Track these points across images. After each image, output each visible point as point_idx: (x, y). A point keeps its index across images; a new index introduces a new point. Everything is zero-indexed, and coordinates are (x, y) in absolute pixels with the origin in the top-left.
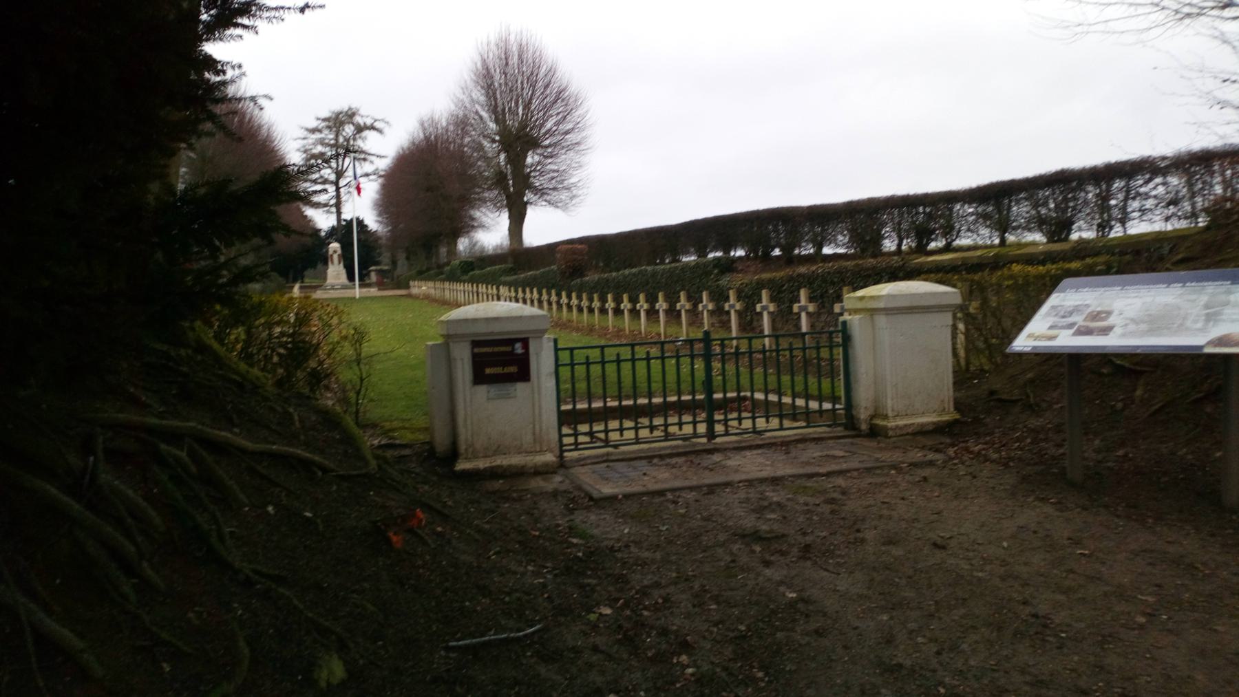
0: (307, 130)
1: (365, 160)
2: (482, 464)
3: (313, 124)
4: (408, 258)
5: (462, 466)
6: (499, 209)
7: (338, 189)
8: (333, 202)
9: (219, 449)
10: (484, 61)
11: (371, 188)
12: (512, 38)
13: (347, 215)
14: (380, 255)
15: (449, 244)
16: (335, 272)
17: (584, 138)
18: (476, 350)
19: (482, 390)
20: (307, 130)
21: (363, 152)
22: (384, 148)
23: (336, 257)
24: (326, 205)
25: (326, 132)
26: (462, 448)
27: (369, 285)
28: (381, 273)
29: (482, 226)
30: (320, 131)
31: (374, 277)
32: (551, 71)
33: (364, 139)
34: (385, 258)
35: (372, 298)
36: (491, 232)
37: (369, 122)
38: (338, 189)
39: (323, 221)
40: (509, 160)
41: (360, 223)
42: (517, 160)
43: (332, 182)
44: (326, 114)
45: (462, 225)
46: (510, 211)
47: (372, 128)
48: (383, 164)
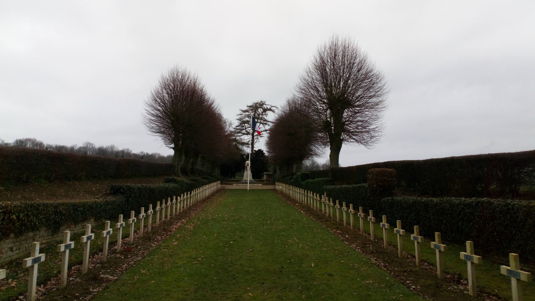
0: (242, 111)
1: (266, 124)
3: (245, 108)
4: (280, 169)
6: (325, 144)
10: (321, 58)
11: (265, 136)
12: (340, 43)
13: (256, 149)
14: (269, 166)
16: (248, 175)
17: (380, 102)
20: (242, 111)
21: (265, 120)
28: (269, 176)
29: (316, 155)
31: (265, 177)
32: (362, 63)
33: (266, 115)
34: (271, 169)
37: (269, 107)
39: (248, 150)
40: (333, 115)
42: (337, 114)
44: (251, 104)
45: (308, 153)
46: (331, 145)
47: (270, 110)
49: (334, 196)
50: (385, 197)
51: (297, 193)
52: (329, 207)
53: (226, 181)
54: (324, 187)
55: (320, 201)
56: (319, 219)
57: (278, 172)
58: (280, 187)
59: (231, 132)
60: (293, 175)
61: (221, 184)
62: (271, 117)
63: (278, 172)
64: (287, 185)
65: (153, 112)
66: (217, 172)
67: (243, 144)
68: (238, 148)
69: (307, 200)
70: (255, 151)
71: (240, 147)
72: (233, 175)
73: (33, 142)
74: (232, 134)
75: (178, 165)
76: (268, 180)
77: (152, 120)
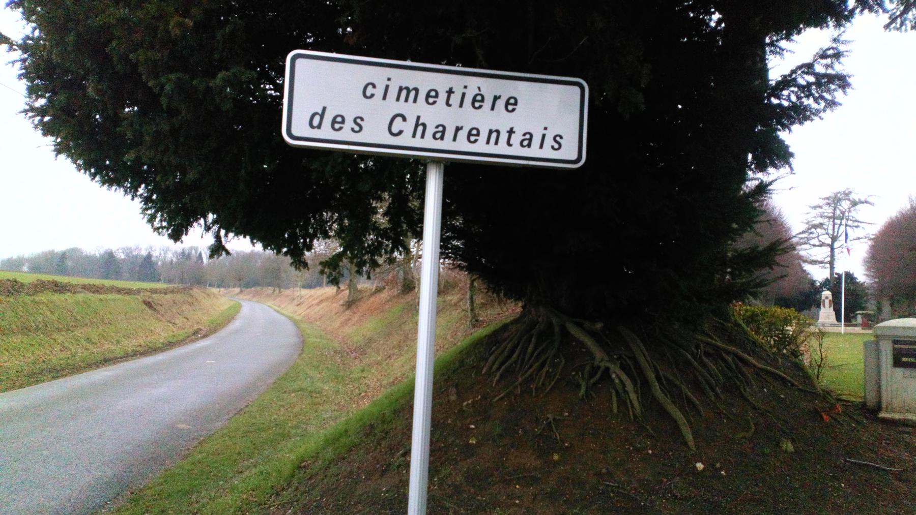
2: (897, 416)
4: (891, 305)
5: (882, 415)
7: (832, 249)
8: (829, 259)
9: (746, 363)
13: (840, 269)
14: (866, 301)
16: (826, 314)
18: (896, 346)
19: (899, 371)
21: (856, 221)
22: (875, 219)
23: (827, 302)
24: (822, 262)
25: (826, 207)
26: (884, 405)
27: (855, 326)
28: (866, 316)
30: (820, 207)
31: (859, 319)
38: (832, 249)
39: (819, 274)
41: (849, 277)
43: (828, 245)
47: (866, 202)
48: (874, 230)
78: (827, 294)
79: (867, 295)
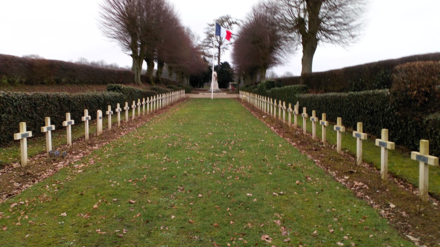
0: (209, 25)
4: (244, 79)
7: (219, 49)
11: (231, 48)
13: (222, 61)
14: (234, 77)
15: (261, 72)
16: (214, 84)
20: (209, 25)
28: (234, 85)
31: (230, 87)
34: (236, 79)
35: (223, 99)
36: (289, 64)
37: (234, 21)
38: (219, 49)
49: (310, 106)
50: (433, 112)
51: (263, 103)
52: (293, 116)
53: (196, 90)
54: (297, 95)
55: (277, 108)
56: (302, 143)
57: (242, 81)
58: (244, 95)
59: (199, 45)
60: (256, 84)
61: (186, 93)
62: (235, 30)
63: (242, 81)
64: (251, 94)
65: (107, 15)
66: (186, 81)
67: (210, 56)
68: (205, 59)
69: (277, 111)
70: (221, 63)
71: (207, 59)
72: (202, 85)
73: (33, 56)
74: (199, 47)
75: (137, 73)
76: (233, 90)
77: (106, 24)
78: (214, 73)
79: (234, 74)
